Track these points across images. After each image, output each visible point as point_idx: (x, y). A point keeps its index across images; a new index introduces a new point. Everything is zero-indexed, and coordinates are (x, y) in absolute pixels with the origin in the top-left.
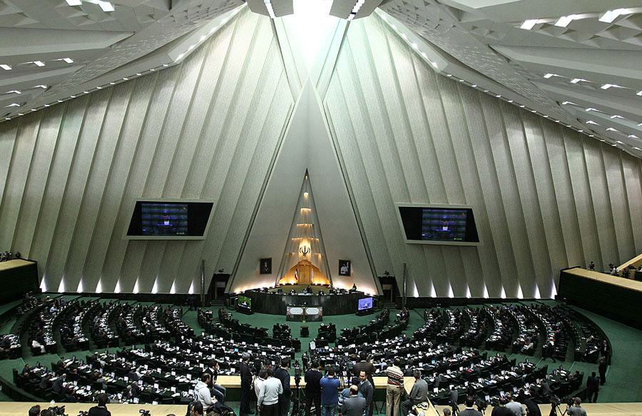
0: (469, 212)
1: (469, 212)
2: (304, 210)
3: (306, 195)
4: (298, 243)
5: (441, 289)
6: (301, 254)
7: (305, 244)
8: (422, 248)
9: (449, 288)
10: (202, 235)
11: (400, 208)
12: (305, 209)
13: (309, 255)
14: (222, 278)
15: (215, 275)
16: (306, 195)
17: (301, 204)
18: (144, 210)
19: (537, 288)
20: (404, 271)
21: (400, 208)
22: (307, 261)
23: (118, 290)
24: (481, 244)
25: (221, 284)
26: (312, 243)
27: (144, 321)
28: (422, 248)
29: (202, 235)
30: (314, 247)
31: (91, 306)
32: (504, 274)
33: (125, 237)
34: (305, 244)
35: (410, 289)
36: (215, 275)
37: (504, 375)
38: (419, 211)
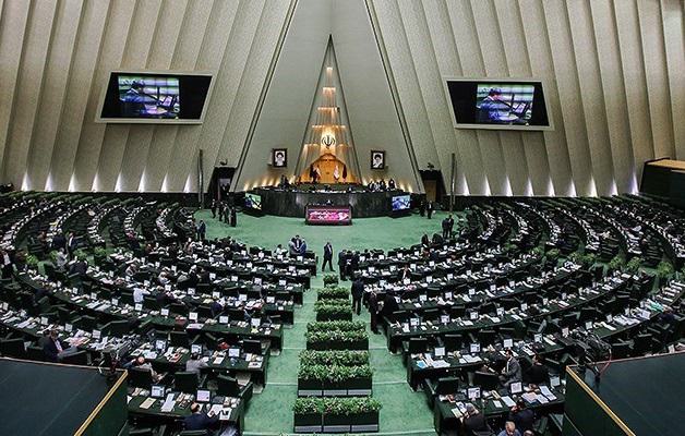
0: (538, 86)
1: (538, 86)
2: (327, 90)
3: (329, 69)
4: (321, 131)
5: (496, 184)
6: (323, 146)
7: (328, 134)
8: (498, 135)
9: (463, 182)
10: (198, 118)
11: (448, 82)
12: (329, 89)
13: (333, 147)
14: (224, 172)
15: (216, 168)
16: (329, 69)
17: (318, 100)
18: (122, 80)
19: (530, 184)
20: (453, 164)
21: (448, 82)
22: (330, 155)
23: (95, 188)
24: (552, 126)
25: (224, 181)
26: (338, 132)
27: (159, 222)
28: (498, 135)
29: (198, 118)
30: (339, 139)
31: (75, 208)
32: (618, 173)
33: (98, 119)
34: (328, 134)
35: (458, 185)
36: (216, 168)
37: (529, 282)
38: (473, 86)
